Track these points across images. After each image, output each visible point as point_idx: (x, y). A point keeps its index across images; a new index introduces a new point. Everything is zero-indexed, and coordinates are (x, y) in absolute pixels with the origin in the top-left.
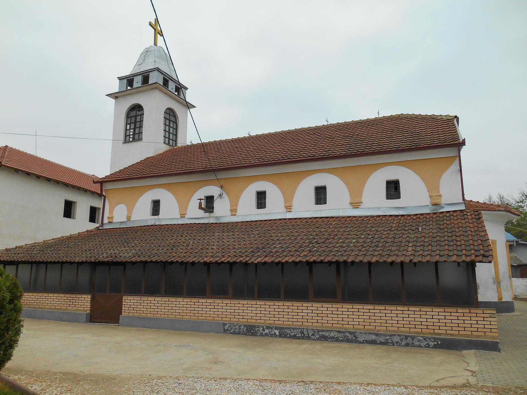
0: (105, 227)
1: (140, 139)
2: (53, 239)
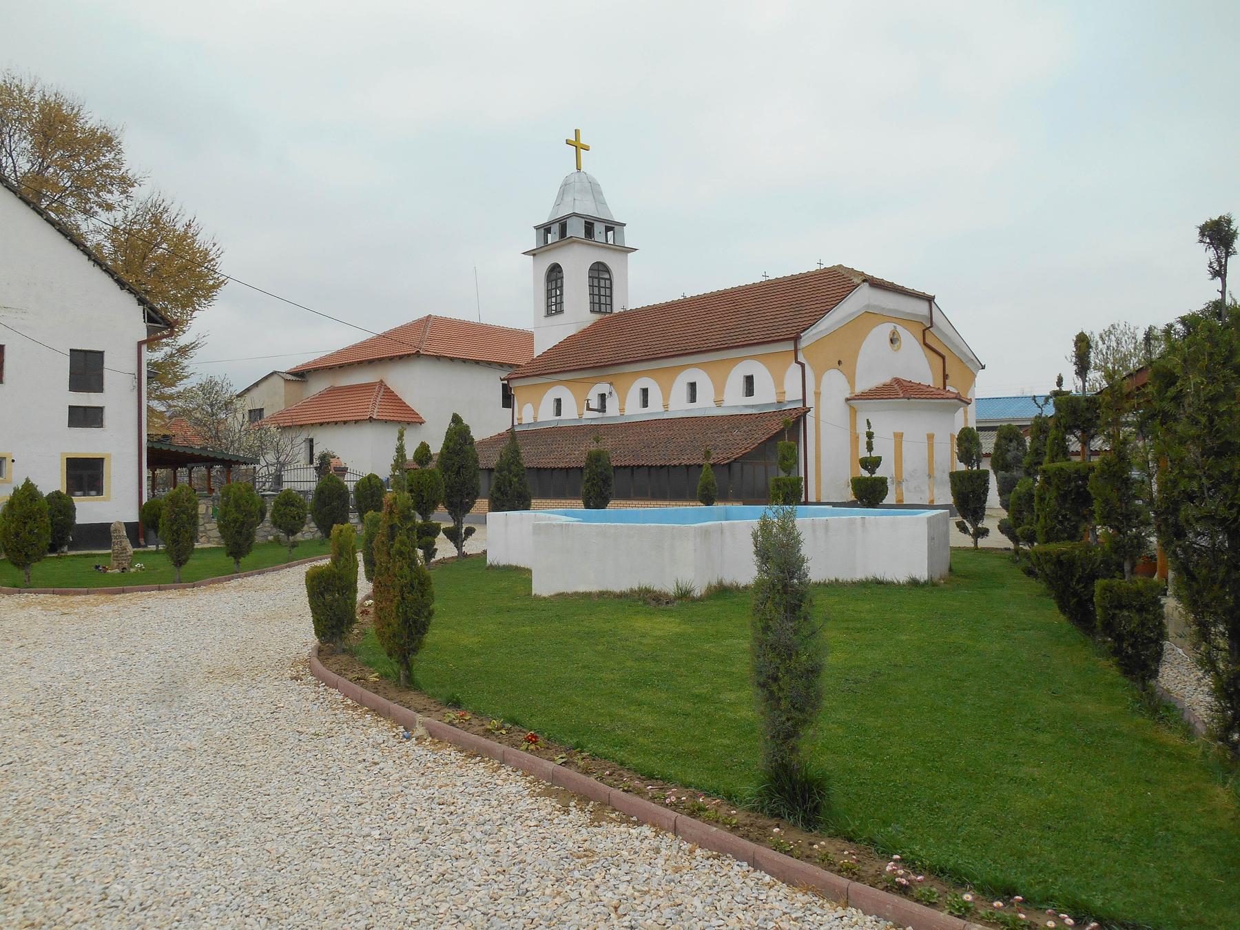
1: (562, 311)
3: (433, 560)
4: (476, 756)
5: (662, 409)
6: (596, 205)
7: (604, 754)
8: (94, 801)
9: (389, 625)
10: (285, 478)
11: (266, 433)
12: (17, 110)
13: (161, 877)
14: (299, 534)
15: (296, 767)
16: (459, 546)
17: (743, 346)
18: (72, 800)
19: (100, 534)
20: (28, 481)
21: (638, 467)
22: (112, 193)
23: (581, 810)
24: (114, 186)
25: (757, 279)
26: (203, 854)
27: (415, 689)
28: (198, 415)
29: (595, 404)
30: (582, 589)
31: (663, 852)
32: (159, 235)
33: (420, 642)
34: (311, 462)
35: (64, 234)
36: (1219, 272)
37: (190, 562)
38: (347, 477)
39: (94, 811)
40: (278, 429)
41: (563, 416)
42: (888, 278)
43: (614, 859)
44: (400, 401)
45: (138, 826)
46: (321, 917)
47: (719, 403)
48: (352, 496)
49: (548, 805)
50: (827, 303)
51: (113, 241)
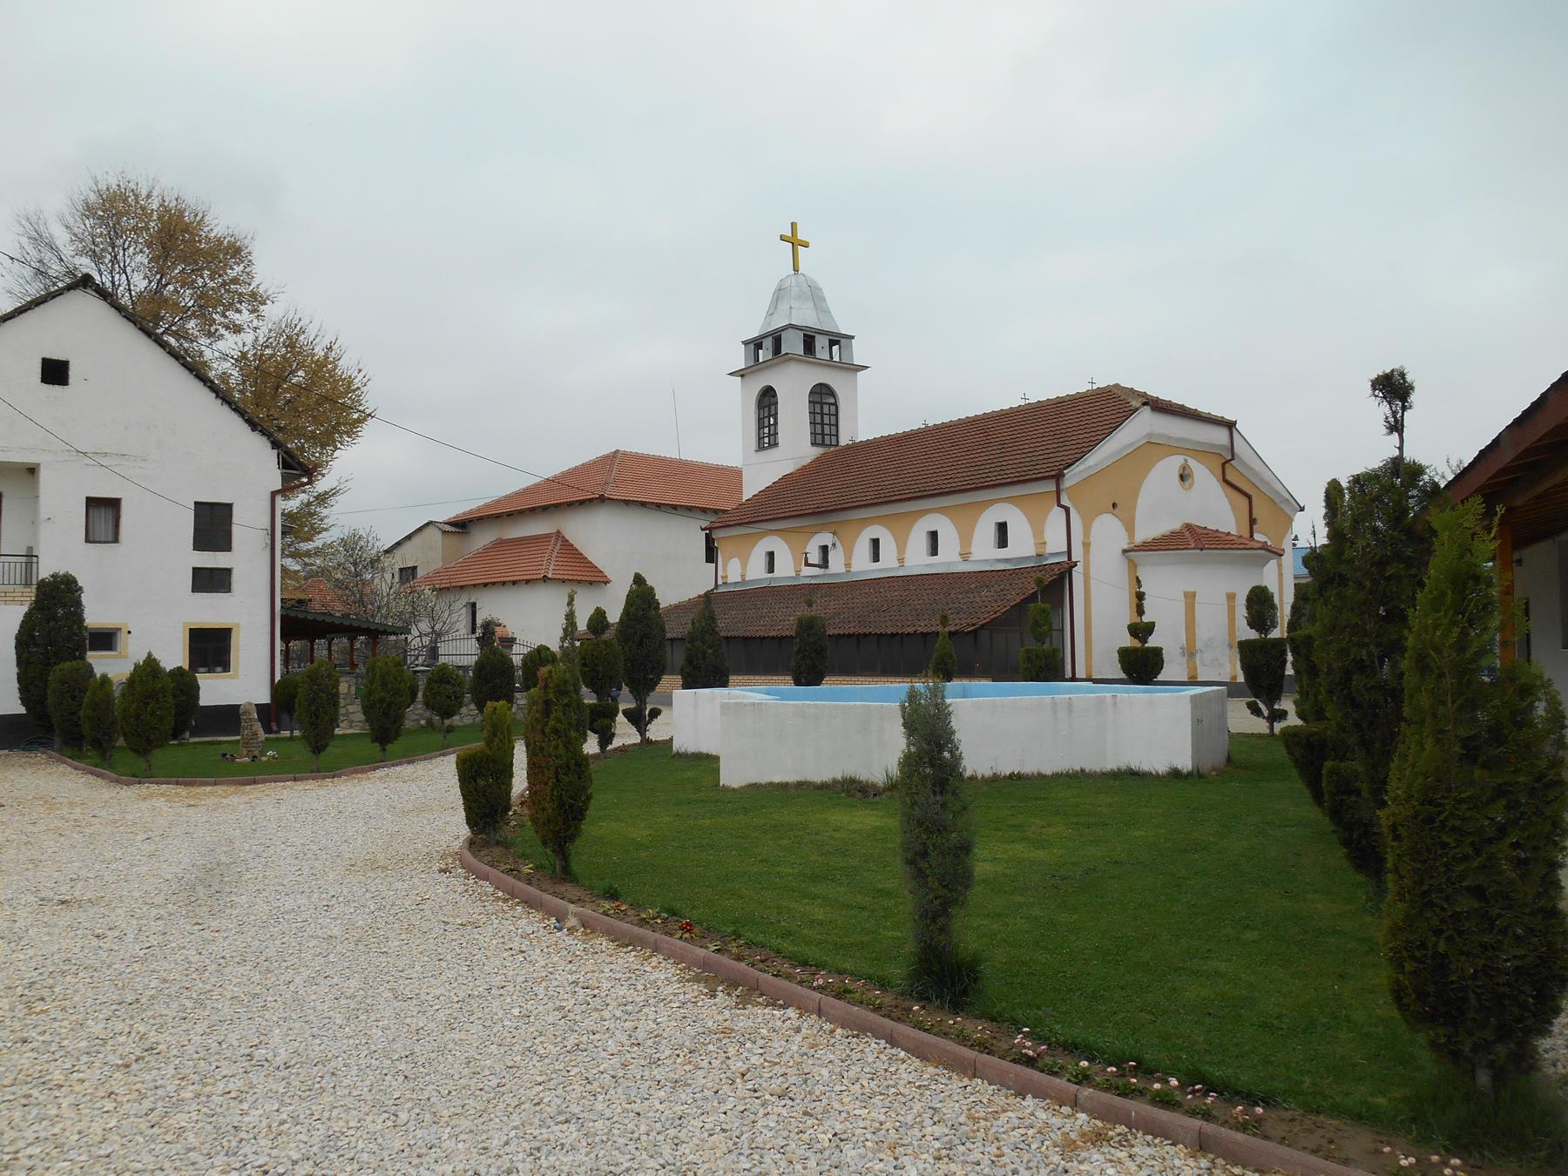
1: (776, 444)
3: (610, 747)
4: (627, 946)
5: (896, 564)
6: (817, 314)
7: (761, 942)
8: (235, 981)
9: (543, 809)
10: (441, 651)
11: (419, 597)
12: (133, 219)
13: (304, 1044)
14: (456, 718)
15: (440, 954)
16: (642, 730)
17: (993, 486)
18: (213, 980)
19: (228, 717)
20: (150, 655)
21: (865, 635)
22: (240, 312)
23: (729, 994)
24: (243, 304)
25: (1016, 402)
26: (343, 1026)
27: (572, 881)
28: (339, 576)
29: (815, 558)
30: (777, 779)
31: (804, 1031)
32: (294, 361)
33: (577, 828)
34: (474, 631)
35: (188, 369)
36: (1396, 427)
37: (329, 749)
38: (516, 649)
39: (235, 989)
40: (433, 591)
41: (777, 574)
42: (1177, 399)
43: (752, 1036)
44: (581, 557)
45: (280, 1003)
46: (456, 1077)
47: (965, 556)
48: (520, 672)
49: (694, 989)
50: (1098, 432)
51: (241, 369)
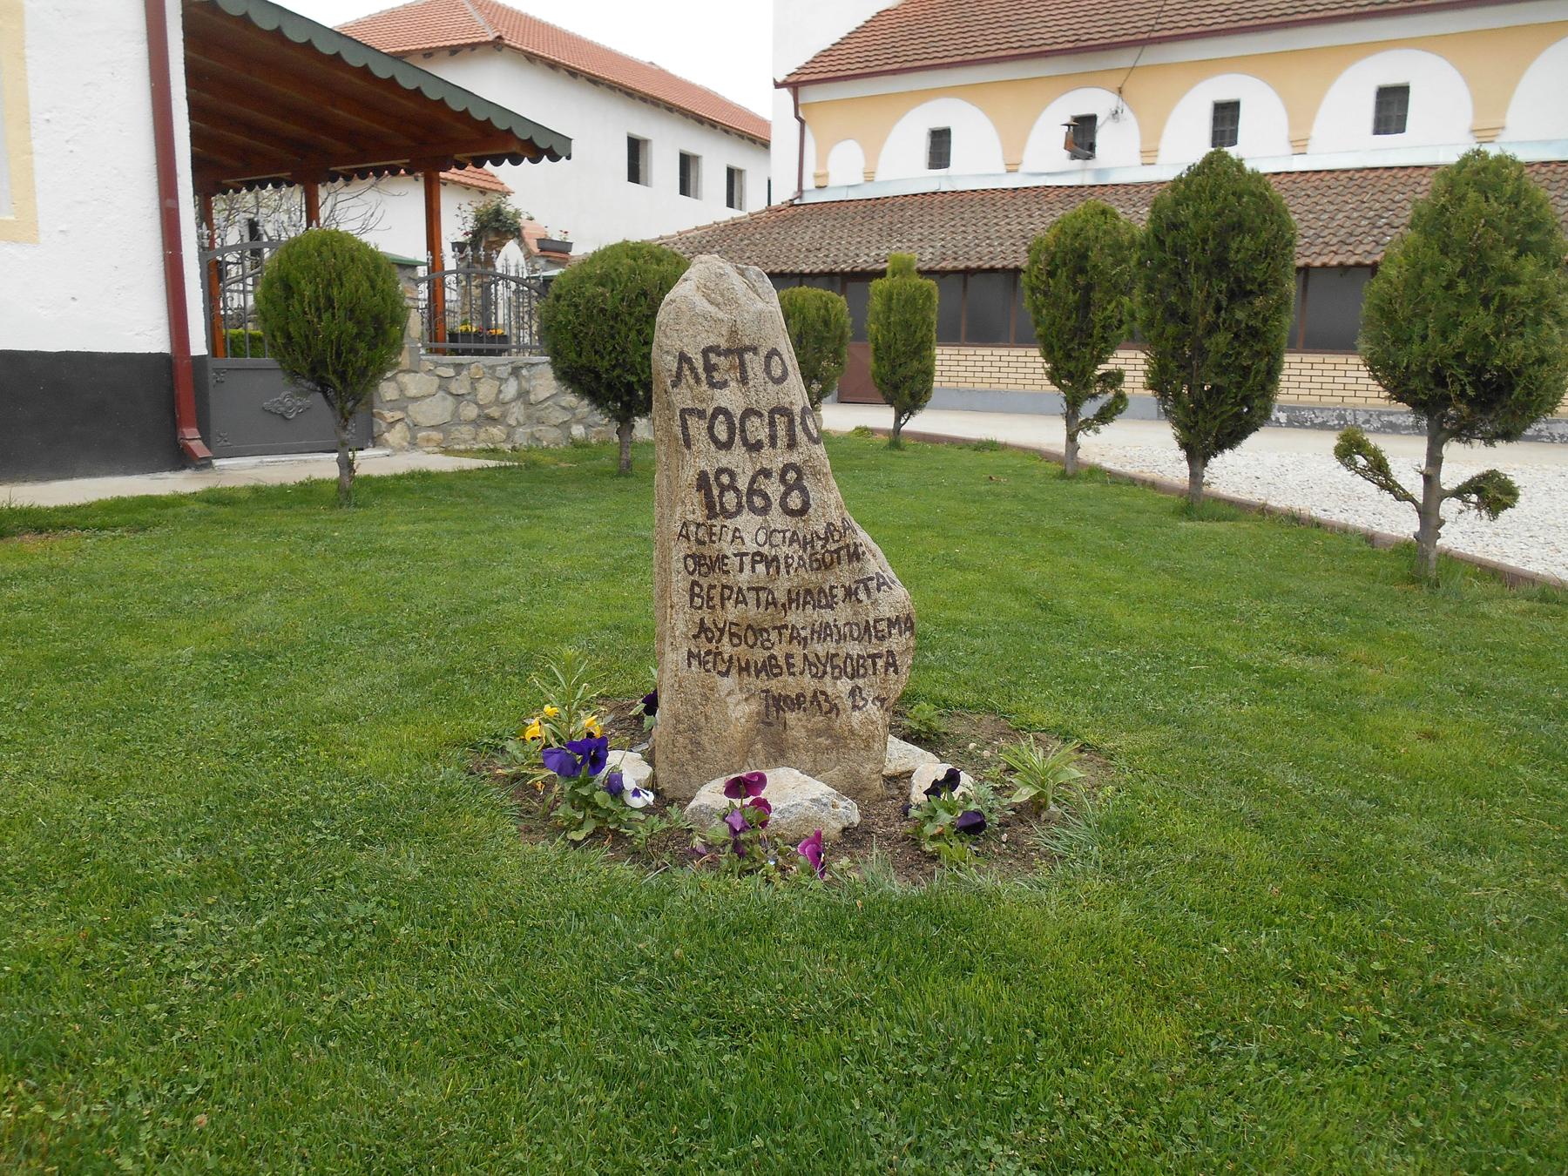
0: (808, 199)
2: (697, 229)
